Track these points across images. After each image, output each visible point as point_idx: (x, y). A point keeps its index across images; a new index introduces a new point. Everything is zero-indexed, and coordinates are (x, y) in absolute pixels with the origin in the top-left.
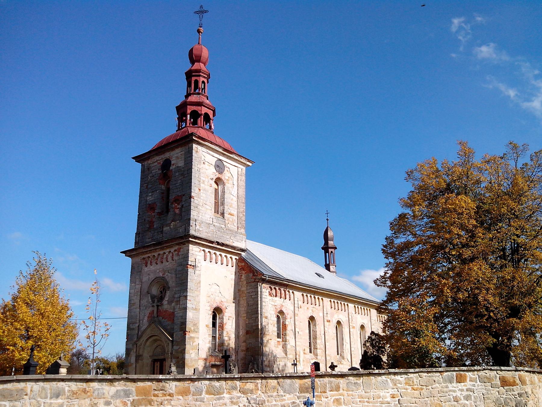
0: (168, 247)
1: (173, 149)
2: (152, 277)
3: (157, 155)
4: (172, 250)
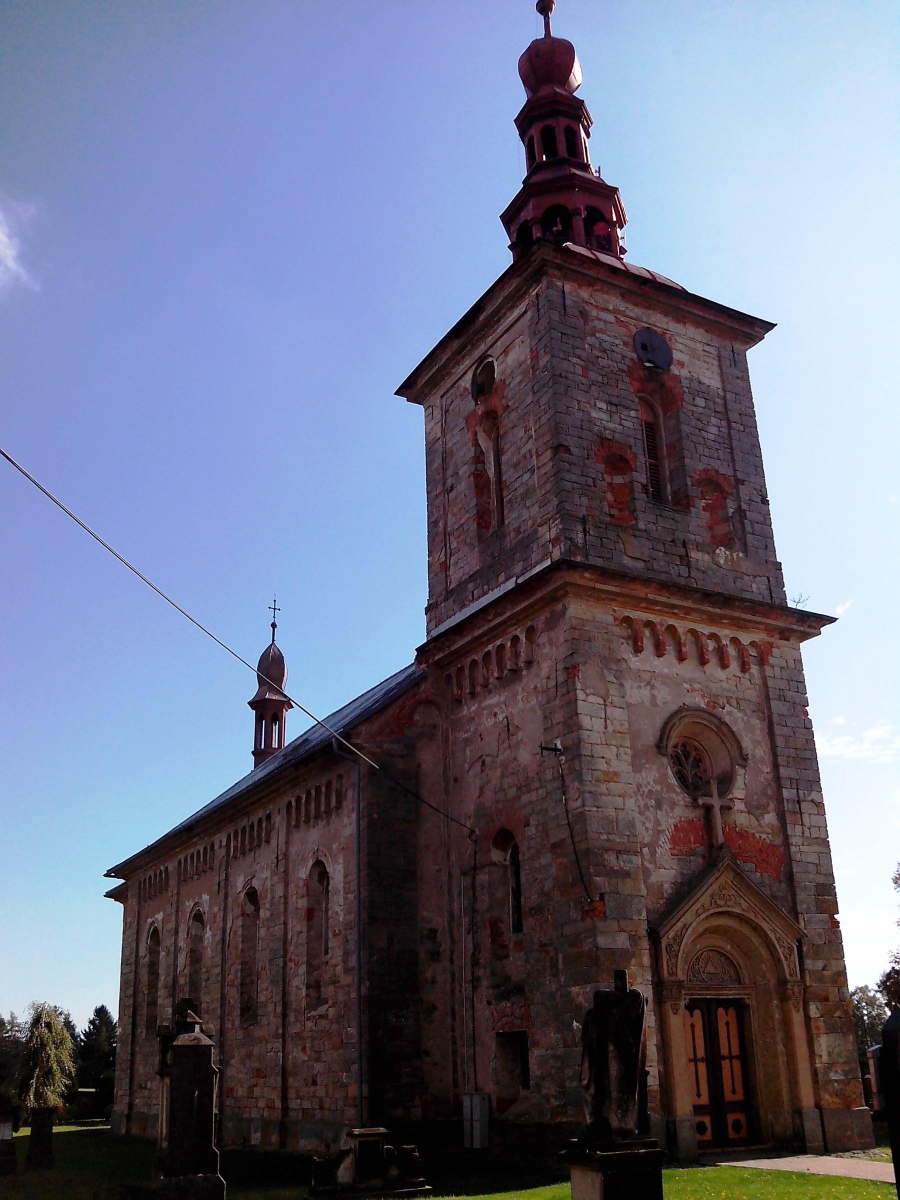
3: (625, 295)
4: (745, 638)
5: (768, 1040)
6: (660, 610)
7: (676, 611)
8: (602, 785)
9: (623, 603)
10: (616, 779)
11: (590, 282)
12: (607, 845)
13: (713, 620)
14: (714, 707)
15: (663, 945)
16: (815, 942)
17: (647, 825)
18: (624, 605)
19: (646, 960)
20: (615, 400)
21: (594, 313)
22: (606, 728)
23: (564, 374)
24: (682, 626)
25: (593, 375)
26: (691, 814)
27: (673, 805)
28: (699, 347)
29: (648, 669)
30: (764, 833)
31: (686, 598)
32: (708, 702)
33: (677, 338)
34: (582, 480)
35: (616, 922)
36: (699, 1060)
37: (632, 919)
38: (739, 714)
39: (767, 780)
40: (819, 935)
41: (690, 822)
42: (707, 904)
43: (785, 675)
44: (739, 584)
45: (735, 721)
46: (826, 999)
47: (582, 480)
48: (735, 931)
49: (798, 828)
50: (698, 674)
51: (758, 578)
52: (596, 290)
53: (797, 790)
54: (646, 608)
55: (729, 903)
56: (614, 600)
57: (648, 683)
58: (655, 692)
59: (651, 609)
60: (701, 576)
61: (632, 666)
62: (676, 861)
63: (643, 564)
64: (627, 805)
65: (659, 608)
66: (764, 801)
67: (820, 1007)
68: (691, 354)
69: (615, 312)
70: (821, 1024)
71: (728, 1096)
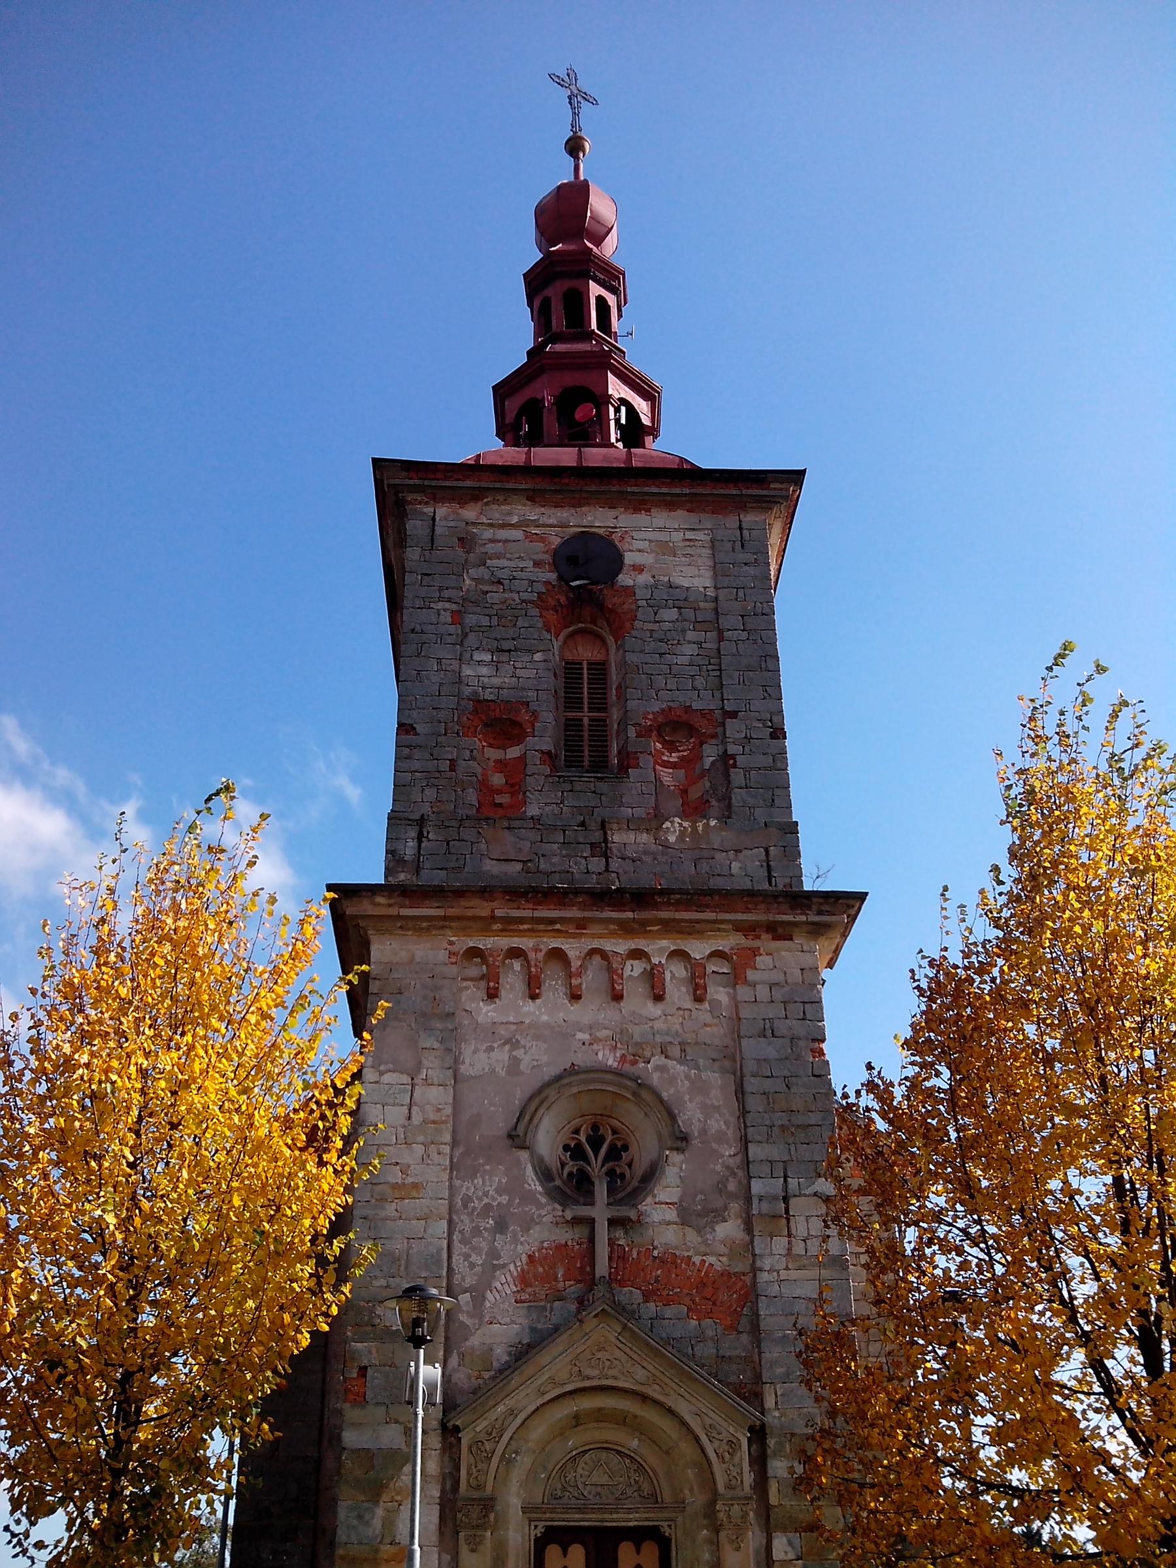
0: (670, 928)
1: (640, 505)
2: (539, 1060)
3: (533, 497)
4: (698, 949)
6: (529, 930)
7: (558, 926)
8: (387, 1205)
10: (414, 1194)
11: (475, 496)
13: (626, 929)
14: (634, 1063)
15: (465, 1443)
16: (796, 1431)
17: (473, 1258)
18: (465, 932)
20: (506, 645)
21: (488, 534)
22: (409, 1118)
23: (418, 628)
24: (573, 949)
25: (470, 620)
26: (566, 1236)
27: (528, 1224)
28: (678, 536)
29: (511, 1019)
30: (712, 1254)
32: (623, 1056)
33: (634, 534)
34: (431, 765)
35: (384, 1408)
38: (681, 1069)
39: (728, 1168)
41: (561, 1248)
42: (563, 1375)
43: (778, 995)
44: (704, 867)
45: (673, 1080)
47: (431, 765)
48: (635, 1417)
50: (609, 1015)
51: (745, 852)
52: (487, 504)
53: (786, 1177)
54: (502, 930)
56: (443, 927)
58: (519, 1053)
59: (512, 930)
60: (630, 867)
61: (480, 1020)
62: (523, 1312)
63: (518, 867)
64: (430, 1231)
65: (526, 927)
66: (719, 1203)
67: (797, 1542)
68: (660, 551)
69: (522, 524)
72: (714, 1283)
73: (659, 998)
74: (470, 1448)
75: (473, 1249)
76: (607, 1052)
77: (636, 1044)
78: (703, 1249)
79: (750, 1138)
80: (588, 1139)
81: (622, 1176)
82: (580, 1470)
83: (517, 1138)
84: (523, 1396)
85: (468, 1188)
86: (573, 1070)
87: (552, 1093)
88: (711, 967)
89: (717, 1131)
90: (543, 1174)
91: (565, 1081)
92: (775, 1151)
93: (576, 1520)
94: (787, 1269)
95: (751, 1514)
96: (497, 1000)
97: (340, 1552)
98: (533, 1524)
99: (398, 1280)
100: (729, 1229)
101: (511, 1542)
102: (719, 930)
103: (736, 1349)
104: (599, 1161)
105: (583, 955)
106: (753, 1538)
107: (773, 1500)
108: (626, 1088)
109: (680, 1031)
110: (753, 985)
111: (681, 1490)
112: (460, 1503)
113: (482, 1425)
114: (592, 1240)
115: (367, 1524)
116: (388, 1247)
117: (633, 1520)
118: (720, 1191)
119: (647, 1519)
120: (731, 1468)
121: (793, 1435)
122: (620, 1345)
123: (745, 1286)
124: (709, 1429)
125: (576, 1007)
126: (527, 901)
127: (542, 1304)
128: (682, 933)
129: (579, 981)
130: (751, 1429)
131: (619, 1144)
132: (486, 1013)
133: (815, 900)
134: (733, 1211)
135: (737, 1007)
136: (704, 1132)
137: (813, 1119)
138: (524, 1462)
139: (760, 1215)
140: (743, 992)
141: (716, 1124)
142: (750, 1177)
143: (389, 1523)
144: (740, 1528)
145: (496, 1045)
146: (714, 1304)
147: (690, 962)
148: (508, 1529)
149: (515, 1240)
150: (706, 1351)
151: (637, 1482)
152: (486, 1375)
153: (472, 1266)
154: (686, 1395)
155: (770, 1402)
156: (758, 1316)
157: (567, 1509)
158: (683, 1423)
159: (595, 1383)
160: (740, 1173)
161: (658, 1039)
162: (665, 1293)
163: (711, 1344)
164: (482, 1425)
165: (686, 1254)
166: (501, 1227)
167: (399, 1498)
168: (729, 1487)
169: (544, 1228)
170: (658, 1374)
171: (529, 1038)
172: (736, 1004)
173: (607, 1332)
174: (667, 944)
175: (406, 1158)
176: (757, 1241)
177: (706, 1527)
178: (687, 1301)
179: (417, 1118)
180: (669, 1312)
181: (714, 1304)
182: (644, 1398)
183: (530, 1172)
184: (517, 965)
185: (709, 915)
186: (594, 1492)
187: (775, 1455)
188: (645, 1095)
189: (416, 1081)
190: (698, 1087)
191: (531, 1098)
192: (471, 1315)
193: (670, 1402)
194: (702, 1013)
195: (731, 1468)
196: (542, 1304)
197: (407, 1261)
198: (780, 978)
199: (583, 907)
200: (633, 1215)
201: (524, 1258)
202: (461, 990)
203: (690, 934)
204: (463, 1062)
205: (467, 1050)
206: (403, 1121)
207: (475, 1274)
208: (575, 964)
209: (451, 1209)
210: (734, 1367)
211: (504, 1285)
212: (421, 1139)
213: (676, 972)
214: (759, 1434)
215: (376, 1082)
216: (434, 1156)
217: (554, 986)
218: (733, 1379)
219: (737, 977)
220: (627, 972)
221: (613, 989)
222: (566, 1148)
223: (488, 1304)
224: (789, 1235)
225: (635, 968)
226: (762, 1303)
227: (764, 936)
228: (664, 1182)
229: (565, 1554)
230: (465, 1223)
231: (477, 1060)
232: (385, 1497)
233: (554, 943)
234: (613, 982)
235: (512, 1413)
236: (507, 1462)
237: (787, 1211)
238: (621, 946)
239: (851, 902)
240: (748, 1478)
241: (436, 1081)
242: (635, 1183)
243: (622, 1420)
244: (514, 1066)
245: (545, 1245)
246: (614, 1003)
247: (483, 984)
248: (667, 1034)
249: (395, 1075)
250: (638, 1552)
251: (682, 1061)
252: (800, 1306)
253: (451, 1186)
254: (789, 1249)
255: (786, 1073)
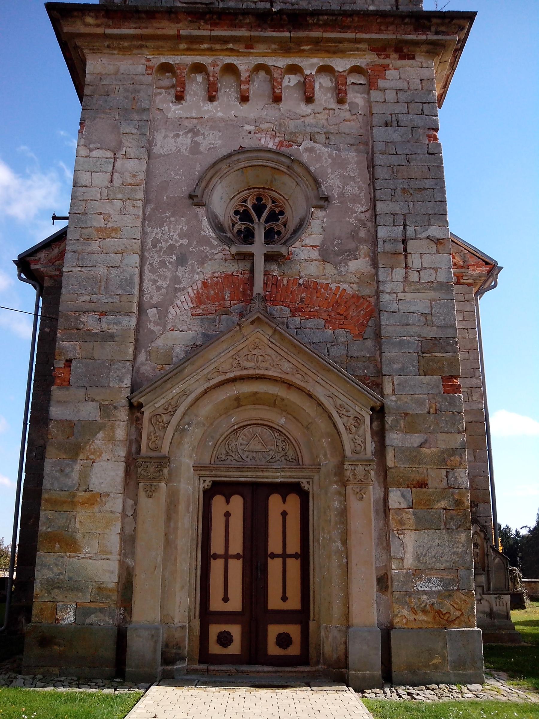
0: (319, 46)
2: (215, 144)
4: (341, 65)
5: (325, 536)
7: (231, 46)
8: (92, 243)
9: (157, 48)
10: (114, 235)
12: (88, 306)
13: (286, 48)
15: (146, 415)
16: (410, 412)
18: (158, 50)
19: (120, 433)
22: (111, 182)
24: (244, 64)
27: (203, 260)
29: (194, 115)
30: (345, 282)
31: (234, 26)
35: (83, 390)
36: (291, 556)
37: (108, 387)
38: (325, 150)
39: (360, 220)
40: (421, 403)
43: (402, 97)
45: (319, 158)
46: (422, 484)
48: (283, 400)
49: (399, 273)
50: (271, 113)
53: (405, 226)
54: (188, 49)
55: (263, 365)
56: (141, 47)
57: (191, 130)
58: (199, 139)
61: (170, 115)
62: (199, 322)
64: (125, 262)
65: (205, 46)
66: (352, 245)
70: (409, 517)
71: (274, 602)
72: (346, 303)
73: (309, 100)
74: (150, 420)
75: (160, 276)
76: (268, 139)
77: (291, 133)
78: (338, 278)
79: (378, 197)
80: (254, 206)
81: (279, 233)
82: (240, 441)
83: (196, 199)
84: (195, 383)
85: (156, 234)
86: (242, 150)
87: (224, 166)
88: (351, 79)
89: (353, 194)
90: (216, 225)
91: (235, 158)
92: (397, 207)
93: (234, 476)
94: (404, 291)
95: (372, 473)
96: (183, 102)
97: (45, 496)
98: (202, 479)
99: (99, 296)
100: (359, 265)
101: (182, 492)
102: (358, 49)
103: (362, 350)
104: (261, 220)
105: (250, 68)
106: (374, 491)
107: (390, 462)
108: (282, 163)
109: (326, 124)
110: (384, 90)
111: (318, 456)
112: (140, 461)
113: (160, 403)
114: (252, 271)
115: (67, 476)
116: (91, 273)
117: (279, 477)
118: (353, 237)
119: (290, 477)
120: (357, 437)
121: (406, 414)
122: (271, 345)
123: (370, 305)
124: (339, 409)
125: (245, 107)
126: (206, 23)
127: (213, 316)
128: (328, 52)
129: (247, 86)
130: (372, 409)
131: (277, 210)
132: (174, 111)
133: (434, 21)
134: (363, 251)
135: (370, 107)
136: (341, 195)
137: (428, 184)
138: (195, 433)
139: (384, 252)
140: (375, 95)
141: (351, 189)
142: (376, 226)
143: (84, 476)
144: (363, 483)
145: (181, 133)
146: (346, 318)
147: (334, 76)
148: (179, 482)
149: (193, 271)
150: (338, 352)
151: (283, 450)
152: (167, 367)
153: (159, 288)
154: (321, 381)
155: (388, 389)
156: (380, 325)
157: (228, 469)
158: (320, 404)
159: (251, 372)
160: (369, 224)
161: (309, 130)
162: (307, 310)
163: (342, 347)
164: (160, 403)
165: (325, 282)
166: (182, 261)
167: (92, 457)
168: (354, 452)
169: (216, 262)
170: (300, 366)
171: (207, 128)
172: (369, 104)
173: (261, 335)
174: (317, 61)
175: (108, 209)
176: (381, 271)
177: (336, 483)
178: (324, 315)
179: (117, 181)
180: (310, 323)
181: (346, 318)
182: (290, 385)
183: (205, 223)
184: (199, 78)
185: (350, 35)
186: (250, 457)
187: (392, 428)
188: (296, 168)
189: (117, 156)
190: (339, 163)
191: (208, 169)
192: (156, 324)
193: (309, 387)
194: (344, 112)
195: (357, 437)
196: (213, 316)
197: (107, 283)
198: (405, 86)
199: (250, 27)
200: (283, 250)
201: (200, 284)
202: (156, 95)
203: (335, 53)
204: (156, 145)
205: (159, 138)
206: (106, 183)
207: (160, 294)
208: (244, 75)
209: (143, 248)
210: (360, 364)
211: (184, 303)
212: (120, 196)
213: (323, 83)
214: (379, 413)
215: (87, 157)
216: (131, 209)
217: (228, 93)
218: (359, 373)
219: (371, 85)
220: (285, 83)
221: (274, 92)
222: (236, 213)
223: (170, 316)
224: (406, 267)
225: (292, 80)
226: (384, 317)
227: (394, 56)
228: (310, 230)
229: (228, 502)
230: (154, 258)
231: (166, 143)
232: (82, 456)
233: (228, 60)
234: (273, 88)
235: (185, 394)
236: (180, 430)
237: (405, 250)
238: (281, 62)
239: (462, 22)
240: (370, 447)
241: (133, 156)
242: (288, 236)
243: (273, 403)
244: (195, 148)
245: (216, 274)
246: (275, 105)
247: (173, 91)
248: (315, 127)
249: (101, 151)
250: (284, 501)
251: (326, 145)
252: (413, 319)
253: (143, 232)
254: (406, 278)
255: (407, 152)
